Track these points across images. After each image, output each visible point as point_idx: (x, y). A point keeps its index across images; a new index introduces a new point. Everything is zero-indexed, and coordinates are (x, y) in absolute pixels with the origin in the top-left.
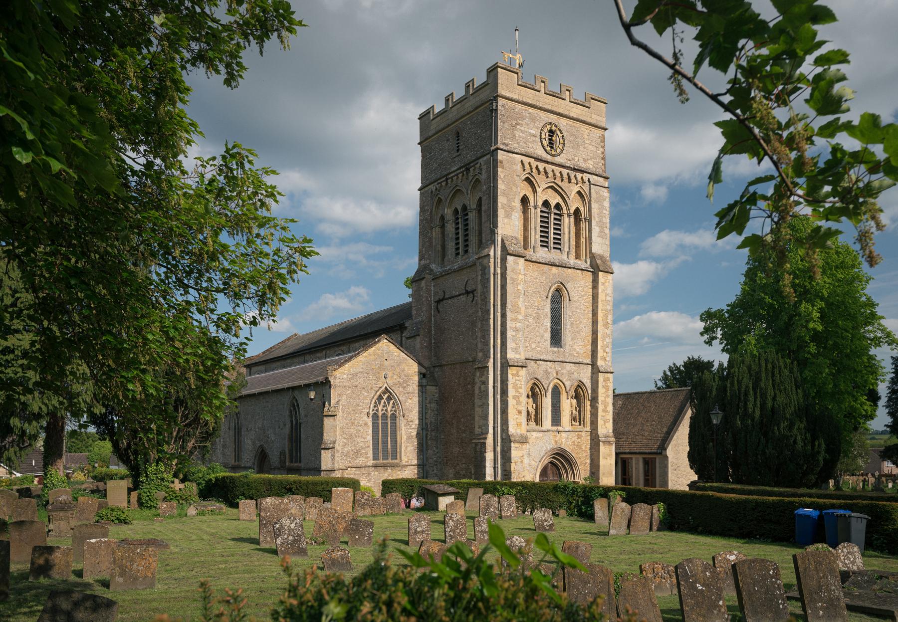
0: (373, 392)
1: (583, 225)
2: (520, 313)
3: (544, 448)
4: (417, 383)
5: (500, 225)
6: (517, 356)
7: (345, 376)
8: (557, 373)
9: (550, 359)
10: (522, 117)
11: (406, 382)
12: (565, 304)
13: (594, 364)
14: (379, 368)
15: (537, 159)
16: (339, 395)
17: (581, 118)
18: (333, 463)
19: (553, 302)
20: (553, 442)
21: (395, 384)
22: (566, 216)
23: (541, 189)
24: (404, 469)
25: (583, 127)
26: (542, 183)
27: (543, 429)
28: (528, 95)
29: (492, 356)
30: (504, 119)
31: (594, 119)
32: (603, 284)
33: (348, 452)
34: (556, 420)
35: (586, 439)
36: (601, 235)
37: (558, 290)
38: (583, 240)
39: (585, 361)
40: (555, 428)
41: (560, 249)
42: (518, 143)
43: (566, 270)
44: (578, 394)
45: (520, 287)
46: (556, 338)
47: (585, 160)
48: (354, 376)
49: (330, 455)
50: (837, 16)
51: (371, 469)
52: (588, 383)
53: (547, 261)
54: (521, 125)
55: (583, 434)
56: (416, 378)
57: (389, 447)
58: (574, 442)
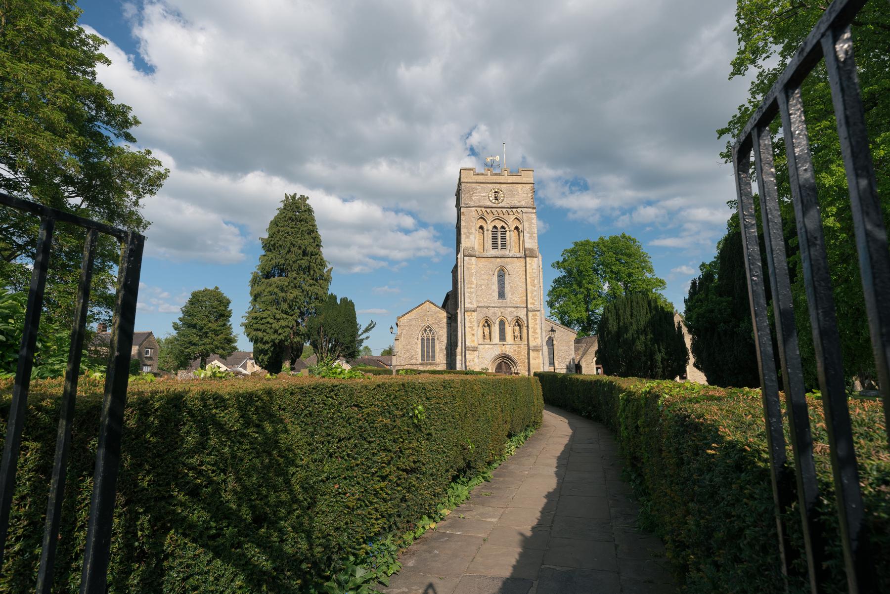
1: (521, 234)
10: (477, 189)
12: (507, 277)
18: (552, 363)
19: (499, 276)
25: (517, 186)
26: (489, 218)
31: (525, 180)
34: (502, 337)
36: (531, 237)
44: (518, 322)
46: (502, 295)
52: (524, 318)
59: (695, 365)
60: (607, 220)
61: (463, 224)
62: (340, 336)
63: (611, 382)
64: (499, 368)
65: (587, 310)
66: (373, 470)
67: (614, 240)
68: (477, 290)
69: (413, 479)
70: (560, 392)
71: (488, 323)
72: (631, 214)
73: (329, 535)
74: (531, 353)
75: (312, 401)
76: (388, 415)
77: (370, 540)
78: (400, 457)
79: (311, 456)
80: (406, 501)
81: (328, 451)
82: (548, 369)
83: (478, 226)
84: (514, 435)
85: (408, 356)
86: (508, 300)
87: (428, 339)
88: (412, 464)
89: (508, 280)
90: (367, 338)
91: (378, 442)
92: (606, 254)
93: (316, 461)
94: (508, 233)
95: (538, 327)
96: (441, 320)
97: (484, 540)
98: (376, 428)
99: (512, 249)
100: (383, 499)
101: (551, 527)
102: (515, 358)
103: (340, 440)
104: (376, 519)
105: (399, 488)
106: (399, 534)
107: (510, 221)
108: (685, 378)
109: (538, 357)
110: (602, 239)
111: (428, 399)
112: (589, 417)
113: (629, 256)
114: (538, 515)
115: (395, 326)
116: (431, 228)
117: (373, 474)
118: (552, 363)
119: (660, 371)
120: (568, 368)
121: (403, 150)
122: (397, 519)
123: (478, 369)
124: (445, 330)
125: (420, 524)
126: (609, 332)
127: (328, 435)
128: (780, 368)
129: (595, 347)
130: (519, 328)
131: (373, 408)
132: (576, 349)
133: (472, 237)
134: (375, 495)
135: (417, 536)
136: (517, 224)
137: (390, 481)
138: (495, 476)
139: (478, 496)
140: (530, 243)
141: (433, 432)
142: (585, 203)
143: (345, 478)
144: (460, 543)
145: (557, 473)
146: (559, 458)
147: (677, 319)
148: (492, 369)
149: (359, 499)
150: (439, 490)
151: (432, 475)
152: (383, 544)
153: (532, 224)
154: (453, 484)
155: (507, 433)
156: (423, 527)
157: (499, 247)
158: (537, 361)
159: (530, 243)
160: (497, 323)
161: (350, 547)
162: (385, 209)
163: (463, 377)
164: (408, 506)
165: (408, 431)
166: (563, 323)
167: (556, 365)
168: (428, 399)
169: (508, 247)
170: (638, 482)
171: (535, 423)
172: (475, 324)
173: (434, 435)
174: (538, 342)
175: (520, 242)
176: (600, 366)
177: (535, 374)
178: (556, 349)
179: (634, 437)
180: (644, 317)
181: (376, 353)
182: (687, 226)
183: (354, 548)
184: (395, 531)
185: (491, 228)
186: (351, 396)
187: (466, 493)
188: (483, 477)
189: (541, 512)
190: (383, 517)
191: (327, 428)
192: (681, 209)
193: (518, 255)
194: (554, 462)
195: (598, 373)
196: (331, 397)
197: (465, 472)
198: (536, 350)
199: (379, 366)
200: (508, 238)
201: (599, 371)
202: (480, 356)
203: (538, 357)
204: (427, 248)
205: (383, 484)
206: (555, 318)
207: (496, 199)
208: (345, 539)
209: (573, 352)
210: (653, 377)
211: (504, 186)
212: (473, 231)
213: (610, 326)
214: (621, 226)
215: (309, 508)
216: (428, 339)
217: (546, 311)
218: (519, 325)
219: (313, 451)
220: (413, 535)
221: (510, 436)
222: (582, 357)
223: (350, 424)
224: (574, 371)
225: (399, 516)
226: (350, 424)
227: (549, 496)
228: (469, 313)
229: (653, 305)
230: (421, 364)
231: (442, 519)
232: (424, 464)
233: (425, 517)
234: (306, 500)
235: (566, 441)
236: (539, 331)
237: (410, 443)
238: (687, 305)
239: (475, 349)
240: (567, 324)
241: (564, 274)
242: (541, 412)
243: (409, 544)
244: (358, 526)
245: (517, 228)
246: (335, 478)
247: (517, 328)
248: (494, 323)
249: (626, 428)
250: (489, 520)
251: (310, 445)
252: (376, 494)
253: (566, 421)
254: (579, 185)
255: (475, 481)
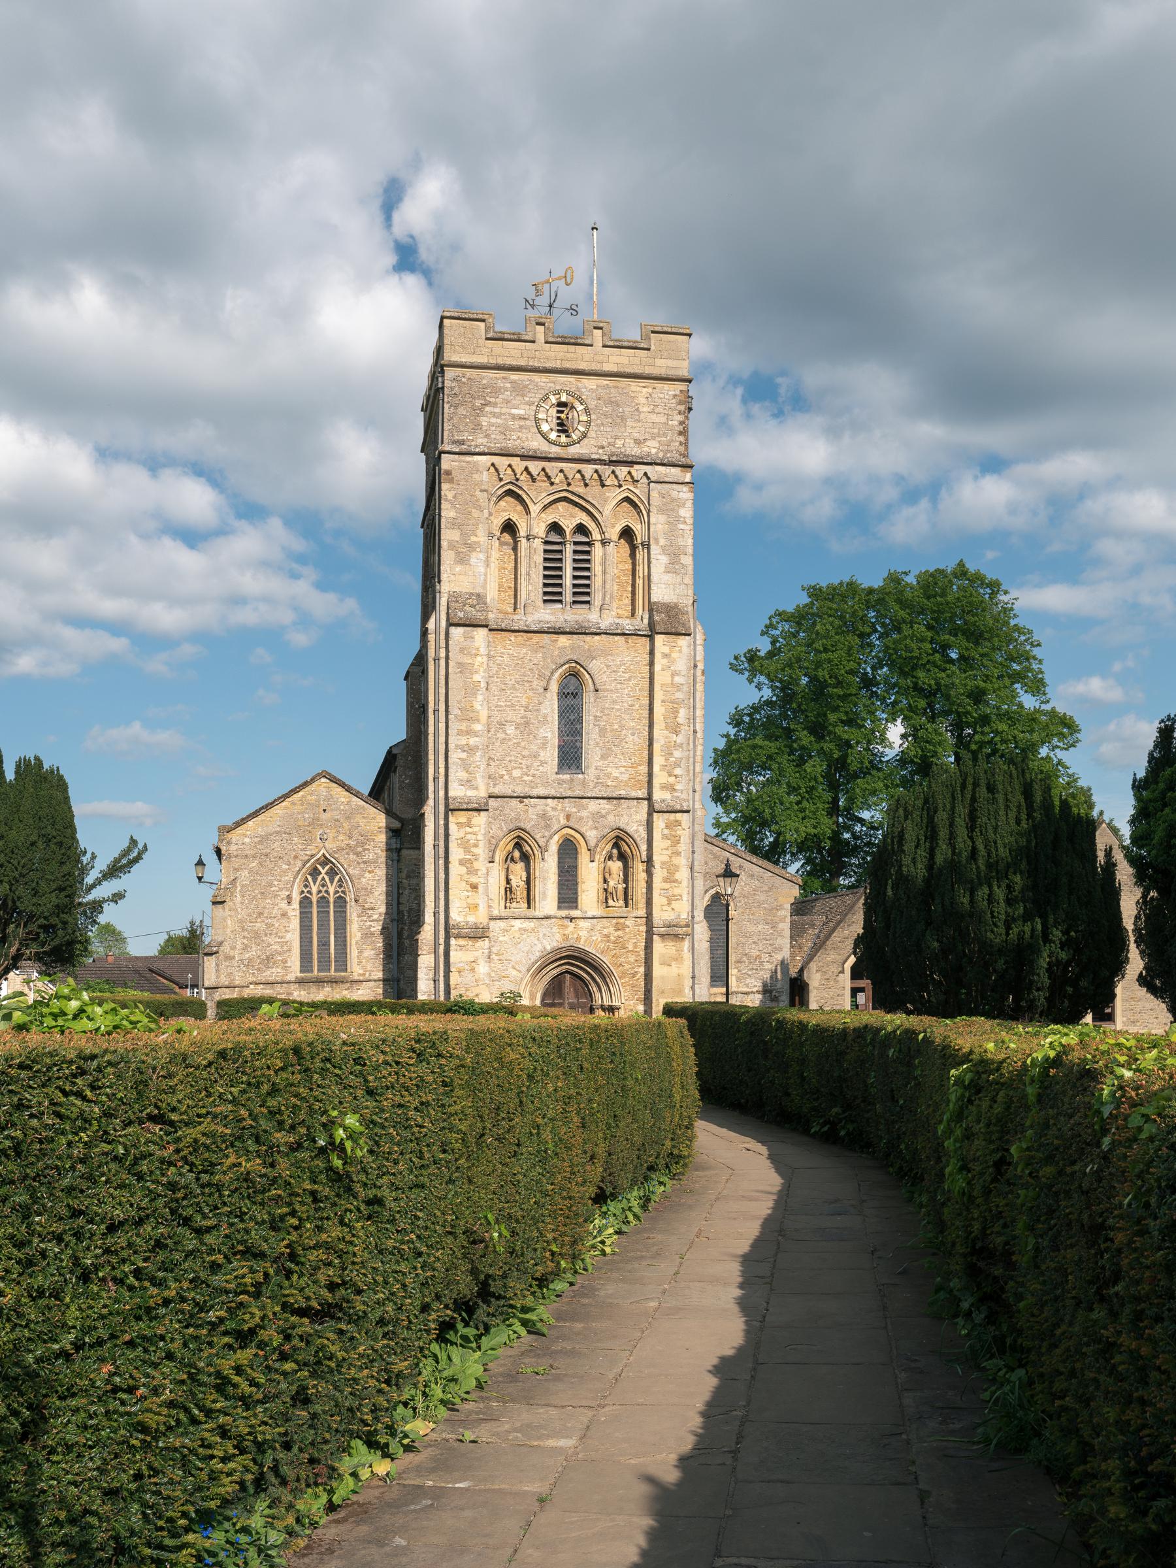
0: (299, 864)
1: (640, 554)
2: (478, 720)
3: (539, 947)
4: (383, 845)
5: (444, 577)
6: (470, 793)
7: (247, 840)
8: (568, 817)
9: (553, 793)
10: (496, 392)
11: (362, 844)
12: (588, 697)
13: (649, 798)
14: (310, 824)
15: (524, 457)
16: (237, 870)
17: (629, 370)
18: (720, 975)
19: (563, 695)
20: (558, 937)
21: (340, 849)
22: (598, 545)
23: (540, 506)
24: (355, 986)
25: (634, 386)
26: (537, 495)
27: (538, 914)
28: (511, 353)
29: (431, 795)
30: (456, 401)
31: (661, 366)
32: (665, 656)
33: (250, 959)
34: (568, 895)
35: (635, 931)
36: (674, 567)
37: (574, 674)
38: (639, 582)
39: (634, 794)
40: (564, 913)
41: (588, 602)
42: (488, 436)
43: (588, 638)
44: (620, 847)
45: (476, 678)
47: (638, 442)
48: (264, 839)
49: (213, 965)
50: (392, 244)
51: (293, 986)
52: (640, 834)
53: (545, 627)
54: (495, 405)
55: (628, 922)
56: (382, 838)
57: (332, 951)
58: (608, 936)
59: (1143, 981)
60: (857, 516)
61: (447, 512)
62: (20, 890)
63: (910, 1034)
64: (554, 992)
65: (834, 810)
66: (212, 1316)
67: (932, 583)
68: (490, 739)
69: (328, 1337)
70: (748, 1065)
71: (521, 850)
72: (934, 500)
73: (87, 1512)
74: (658, 946)
75: (20, 1106)
76: (251, 1145)
77: (206, 1519)
78: (288, 1274)
79: (26, 1281)
80: (306, 1401)
81: (76, 1261)
82: (706, 993)
83: (498, 522)
84: (614, 1197)
85: (258, 952)
86: (591, 774)
87: (323, 901)
88: (325, 1293)
89: (591, 707)
90: (117, 897)
91: (225, 1230)
92: (906, 630)
93: (41, 1293)
94: (598, 551)
95: (682, 862)
96: (366, 838)
97: (542, 1501)
98: (219, 1187)
99: (610, 607)
100: (242, 1398)
101: (735, 1452)
102: (606, 960)
103: (112, 1228)
104: (224, 1460)
105: (289, 1366)
106: (287, 1498)
107: (608, 509)
108: (1110, 1018)
109: (678, 959)
110: (894, 579)
111: (370, 1092)
112: (830, 1138)
113: (975, 636)
114: (696, 1421)
115: (210, 858)
116: (276, 525)
117: (213, 1326)
118: (720, 975)
119: (1041, 998)
120: (768, 991)
121: (154, 241)
122: (281, 1455)
123: (486, 996)
124: (381, 872)
125: (345, 1464)
126: (903, 880)
127: (76, 1213)
128: (331, 1013)
129: (855, 925)
130: (612, 867)
131: (206, 1125)
132: (797, 932)
133: (477, 559)
134: (220, 1389)
135: (336, 1499)
136: (627, 518)
137: (262, 1345)
138: (559, 1316)
139: (512, 1377)
140: (669, 585)
141: (385, 1192)
142: (793, 457)
143: (131, 1344)
144: (468, 1514)
145: (744, 1304)
146: (747, 1260)
147: (1103, 839)
148: (531, 996)
149: (171, 1404)
150: (402, 1366)
151: (382, 1322)
152: (245, 1530)
153: (673, 521)
154: (435, 1347)
155: (592, 1191)
156: (354, 1475)
157: (568, 597)
158: (674, 970)
159: (669, 585)
160: (554, 847)
161: (149, 1545)
162: (105, 455)
163: (438, 1023)
164: (314, 1416)
165: (313, 1193)
166: (755, 850)
167: (733, 981)
168: (370, 1092)
169: (597, 600)
170: (978, 1317)
171: (675, 1158)
172: (482, 851)
173: (389, 1203)
174: (682, 909)
175: (637, 581)
176: (865, 983)
177: (669, 1011)
178: (720, 930)
179: (987, 1192)
180: (1005, 830)
181: (143, 944)
182: (1107, 547)
183: (160, 1547)
184: (276, 1491)
185: (540, 529)
186: (141, 1086)
187: (478, 1370)
188: (524, 1323)
189: (704, 1414)
190: (243, 1451)
191: (70, 1190)
192: (1085, 491)
193: (628, 625)
194: (734, 1271)
195: (855, 1006)
196: (80, 1095)
197: (471, 1311)
198: (674, 933)
199: (155, 988)
200: (597, 568)
201: (861, 998)
202: (492, 956)
203: (678, 959)
204: (267, 599)
205: (243, 1356)
206: (732, 839)
207: (563, 428)
208: (136, 1520)
209: (785, 942)
210: (1015, 1014)
211: (590, 383)
212: (481, 537)
213: (906, 860)
214: (908, 545)
215: (24, 1437)
216: (323, 901)
217: (707, 812)
218: (622, 857)
219: (29, 1263)
220: (324, 1498)
221: (601, 1198)
222: (810, 958)
223: (140, 1177)
224: (785, 998)
225: (287, 1446)
226: (140, 1177)
227: (723, 1368)
228: (462, 817)
229: (1038, 797)
230: (300, 982)
231: (408, 1449)
232: (359, 1292)
233: (358, 1444)
234: (16, 1413)
235: (764, 1207)
236: (683, 874)
237: (320, 1229)
238: (1138, 798)
239: (478, 934)
240: (773, 854)
241: (767, 693)
242: (690, 1126)
243: (314, 1525)
244: (171, 1482)
245: (627, 534)
246: (100, 1343)
247: (616, 866)
248: (544, 850)
249: (964, 1168)
250: (551, 1443)
251: (20, 1245)
252: (222, 1385)
253: (764, 1150)
254: (770, 395)
255: (499, 1336)
